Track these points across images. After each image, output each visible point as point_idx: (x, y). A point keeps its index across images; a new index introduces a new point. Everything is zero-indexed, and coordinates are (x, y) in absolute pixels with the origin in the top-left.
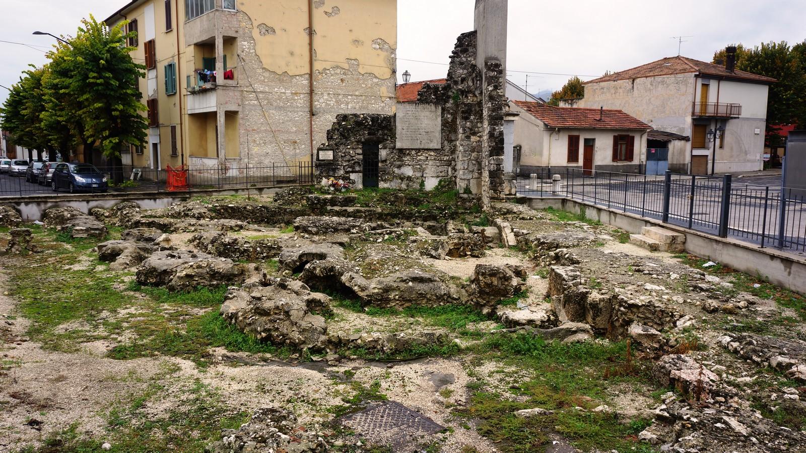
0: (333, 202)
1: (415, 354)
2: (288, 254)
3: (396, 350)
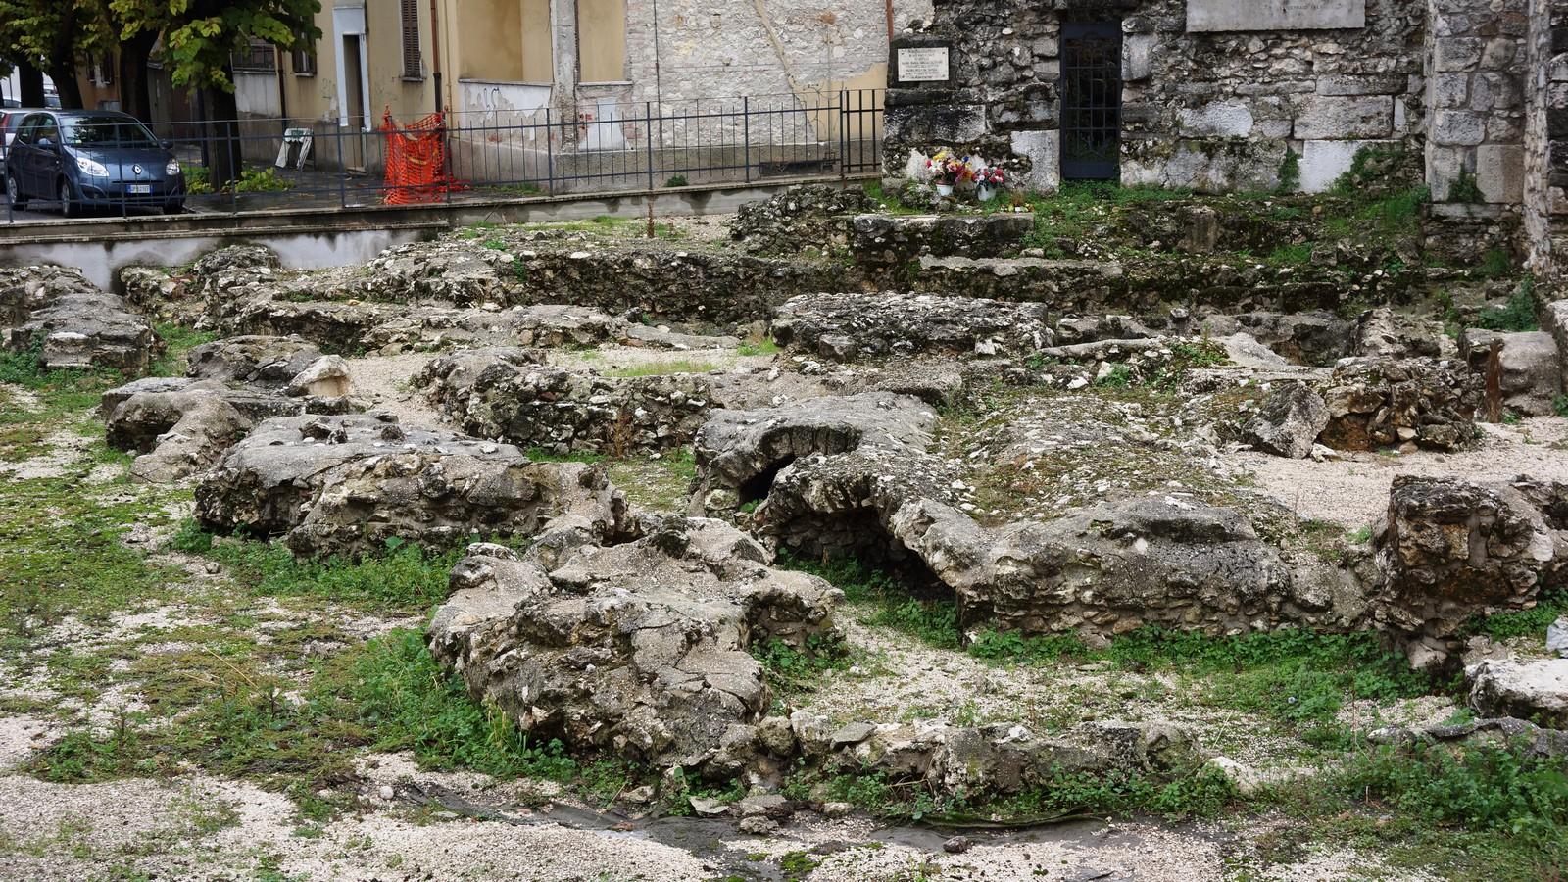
0: (943, 241)
1: (1059, 805)
2: (725, 430)
3: (992, 787)
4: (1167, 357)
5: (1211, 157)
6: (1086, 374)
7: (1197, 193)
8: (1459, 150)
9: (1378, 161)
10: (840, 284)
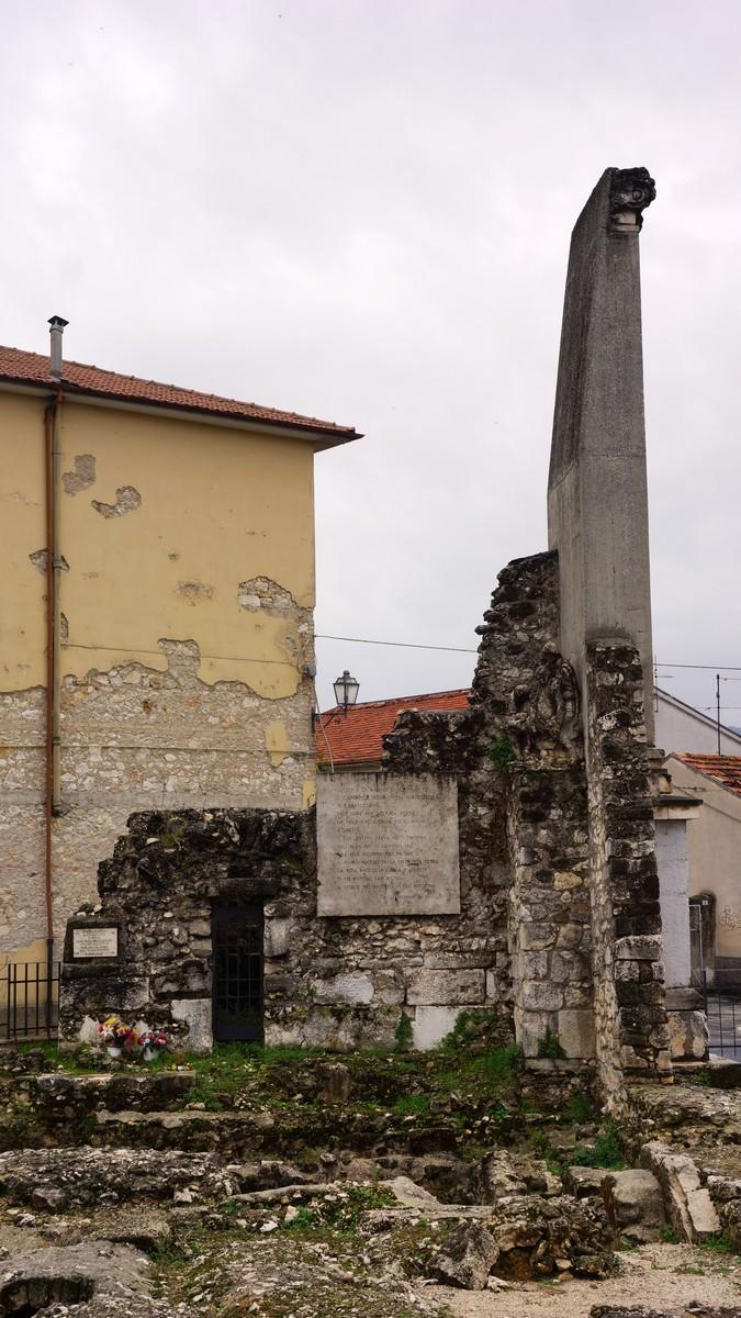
0: (117, 1097)
4: (346, 1201)
5: (340, 1020)
6: (275, 1218)
7: (329, 1051)
8: (544, 1014)
9: (477, 1024)
10: (24, 1139)
